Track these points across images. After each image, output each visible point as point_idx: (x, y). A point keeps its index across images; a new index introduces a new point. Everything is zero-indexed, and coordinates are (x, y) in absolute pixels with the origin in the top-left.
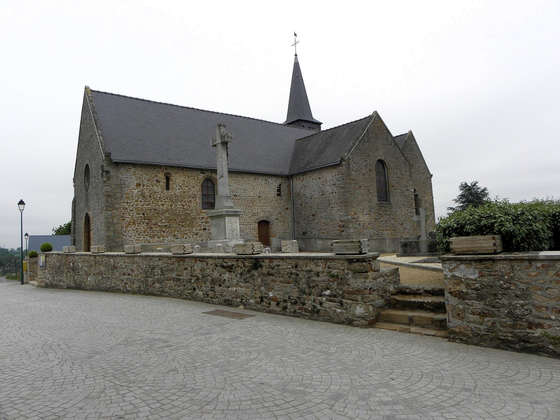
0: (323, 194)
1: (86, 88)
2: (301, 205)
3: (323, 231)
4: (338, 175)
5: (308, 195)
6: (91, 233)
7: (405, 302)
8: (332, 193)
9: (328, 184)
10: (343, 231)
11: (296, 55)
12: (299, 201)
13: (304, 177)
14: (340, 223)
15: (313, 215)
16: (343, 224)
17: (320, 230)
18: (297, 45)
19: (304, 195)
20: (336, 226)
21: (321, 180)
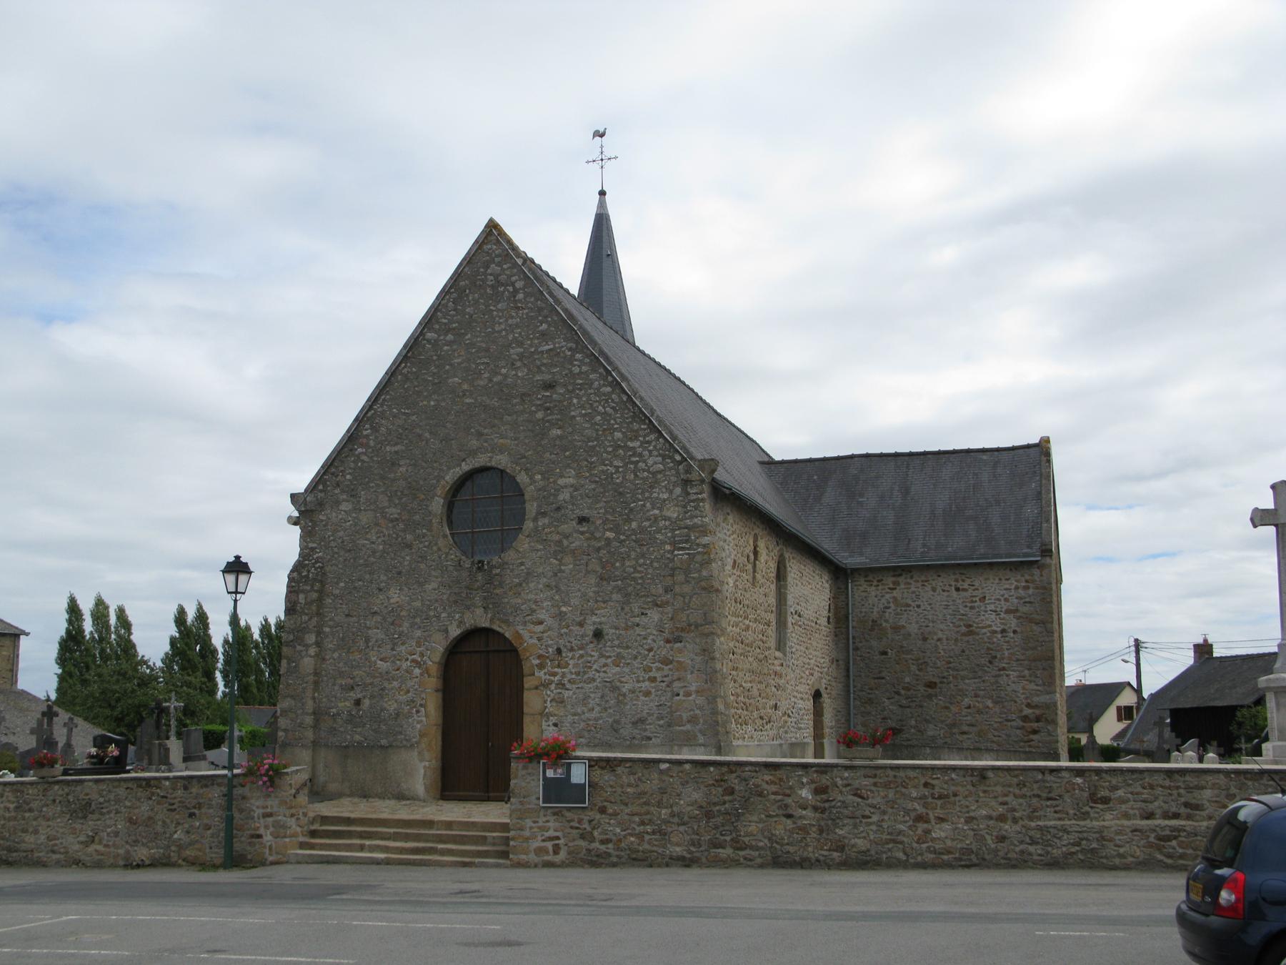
0: (971, 633)
1: (493, 232)
2: (885, 653)
3: (965, 728)
4: (1026, 588)
5: (913, 628)
6: (352, 816)
7: (419, 841)
8: (1003, 631)
9: (992, 607)
10: (1035, 732)
11: (602, 193)
12: (874, 643)
13: (901, 579)
14: (1027, 711)
15: (931, 685)
16: (1038, 712)
17: (953, 725)
18: (607, 164)
19: (896, 629)
20: (1014, 717)
21: (963, 594)
